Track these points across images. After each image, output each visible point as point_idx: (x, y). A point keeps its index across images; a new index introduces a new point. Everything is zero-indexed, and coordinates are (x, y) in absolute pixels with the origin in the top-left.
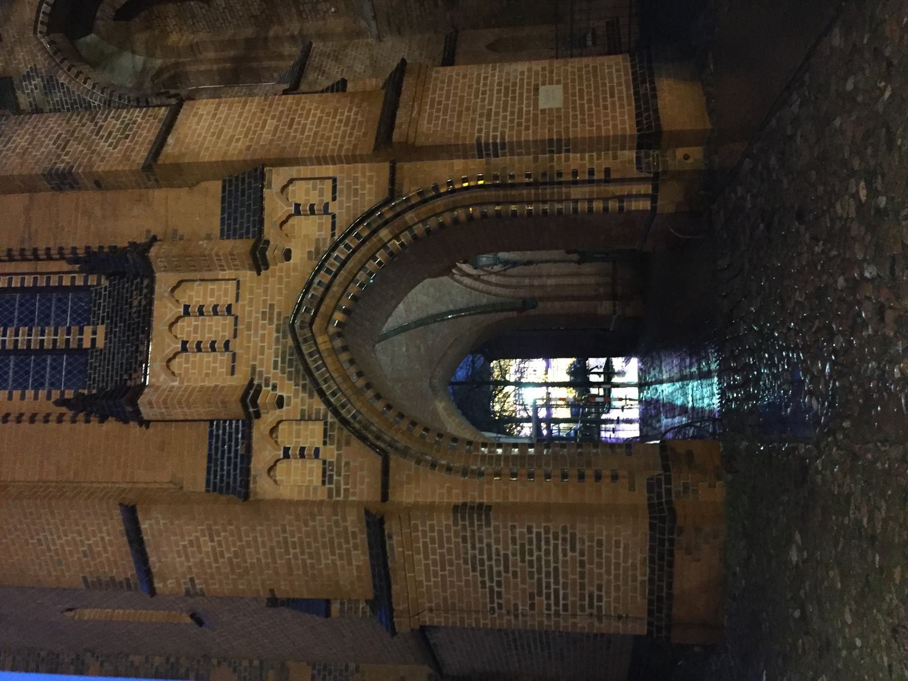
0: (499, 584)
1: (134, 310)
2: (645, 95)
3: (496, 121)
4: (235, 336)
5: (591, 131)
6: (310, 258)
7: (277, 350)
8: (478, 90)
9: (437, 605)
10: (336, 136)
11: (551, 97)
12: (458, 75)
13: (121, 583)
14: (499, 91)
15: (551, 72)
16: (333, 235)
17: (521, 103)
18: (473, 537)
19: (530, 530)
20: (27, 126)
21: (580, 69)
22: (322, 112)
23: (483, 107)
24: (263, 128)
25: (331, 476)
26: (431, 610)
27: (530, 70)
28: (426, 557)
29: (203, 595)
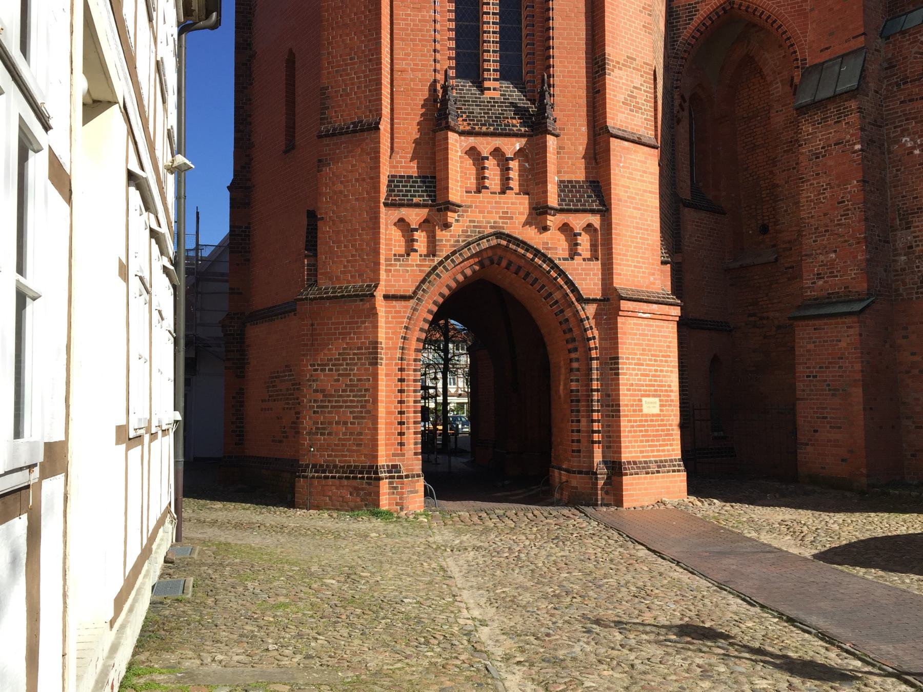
0: (330, 370)
1: (510, 121)
2: (649, 467)
3: (634, 369)
4: (492, 193)
5: (625, 431)
6: (544, 243)
7: (482, 222)
8: (658, 356)
9: (316, 329)
10: (627, 260)
11: (651, 406)
12: (670, 342)
13: (325, 114)
14: (656, 371)
15: (670, 405)
16: (560, 259)
17: (647, 385)
18: (362, 354)
19: (366, 390)
20: (643, 33)
21: (671, 425)
22: (646, 249)
23: (645, 360)
24: (635, 208)
25: (399, 260)
26: (312, 325)
27: (672, 391)
28: (347, 323)
29: (319, 171)
